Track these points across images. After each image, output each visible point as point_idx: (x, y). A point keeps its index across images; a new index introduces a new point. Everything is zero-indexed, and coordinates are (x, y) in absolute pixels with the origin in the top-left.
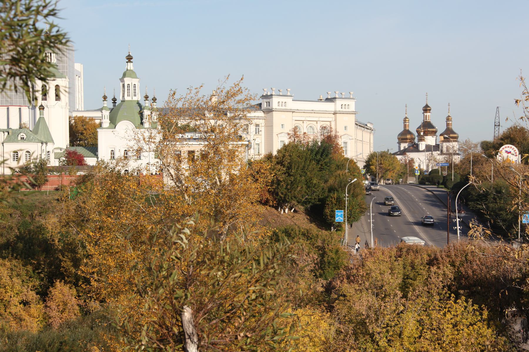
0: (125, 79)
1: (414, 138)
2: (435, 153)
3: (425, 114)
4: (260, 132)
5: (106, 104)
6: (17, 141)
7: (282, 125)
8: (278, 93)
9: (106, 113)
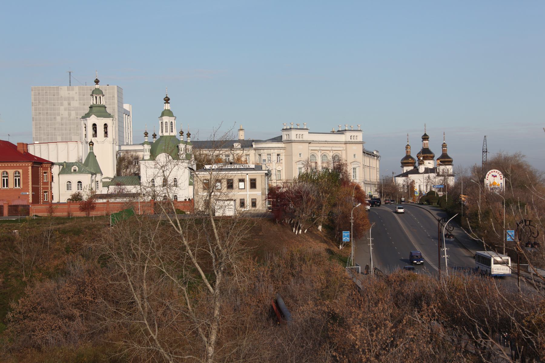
0: (164, 117)
1: (415, 163)
2: (432, 175)
3: (424, 142)
4: (281, 161)
6: (71, 173)
8: (296, 127)
9: (147, 147)
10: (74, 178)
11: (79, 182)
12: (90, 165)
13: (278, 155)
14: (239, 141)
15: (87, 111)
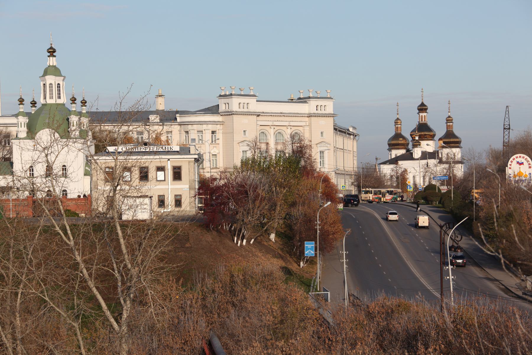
0: (47, 77)
1: (408, 144)
2: (432, 162)
3: (421, 114)
4: (217, 142)
5: (22, 108)
7: (244, 131)
8: (239, 92)
9: (23, 120)
13: (213, 132)
14: (157, 112)
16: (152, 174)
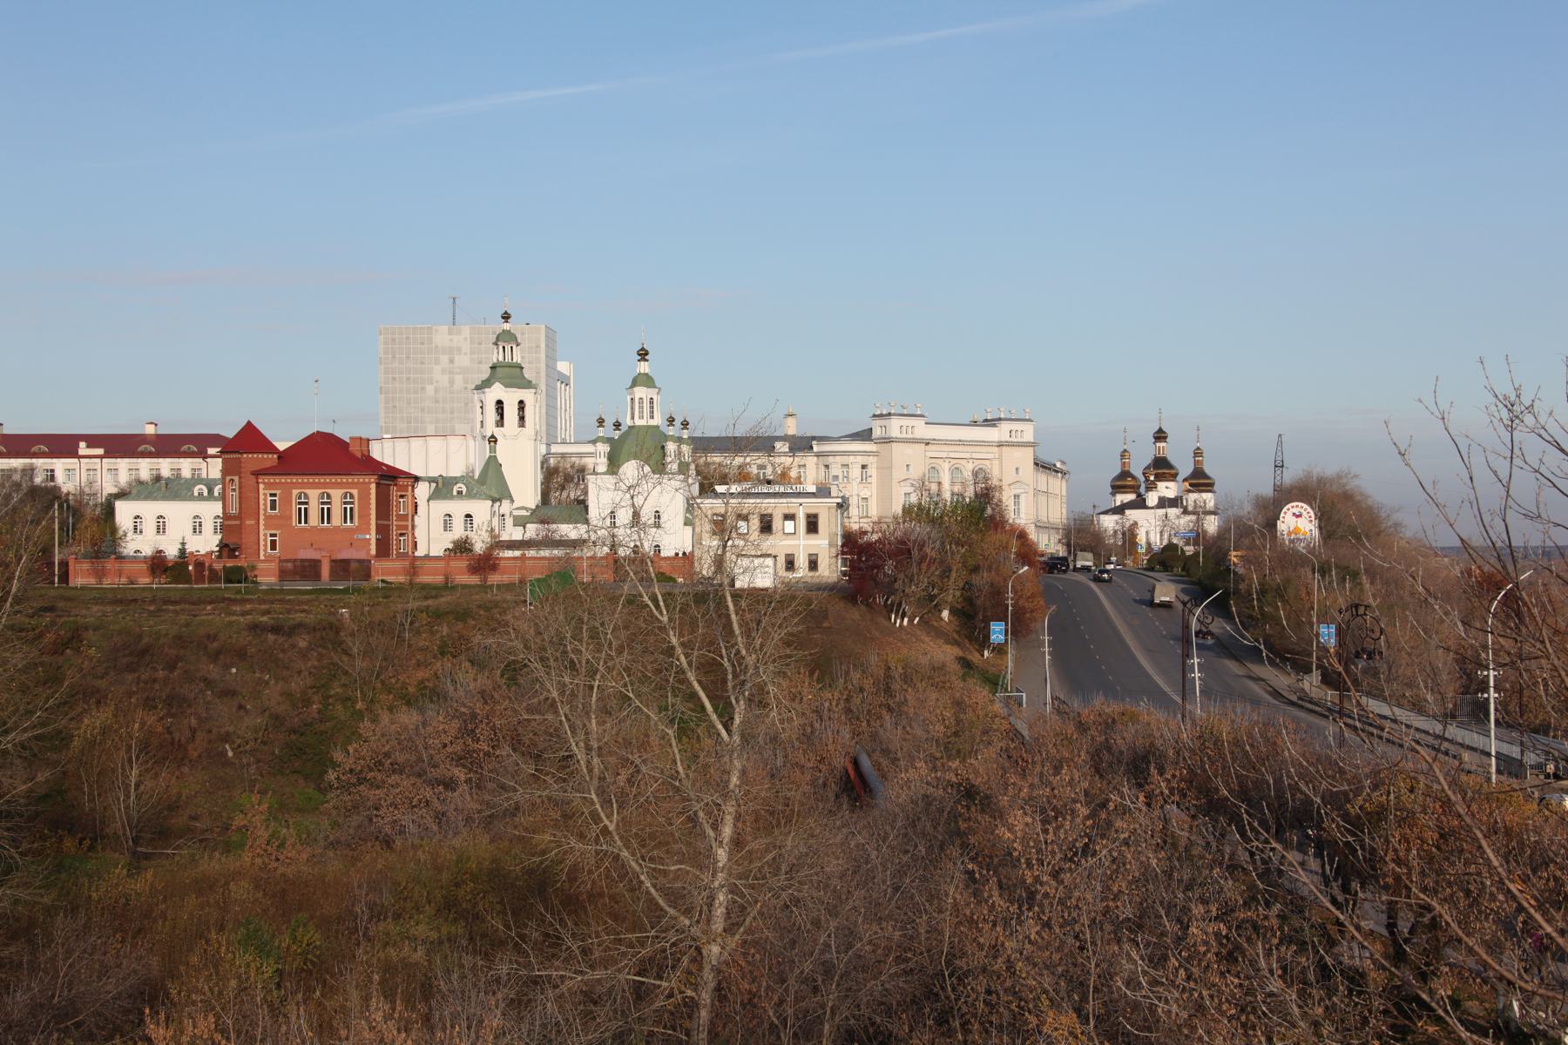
10: (458, 508)
11: (468, 516)
12: (490, 483)
14: (784, 438)
15: (486, 376)
16: (777, 523)
